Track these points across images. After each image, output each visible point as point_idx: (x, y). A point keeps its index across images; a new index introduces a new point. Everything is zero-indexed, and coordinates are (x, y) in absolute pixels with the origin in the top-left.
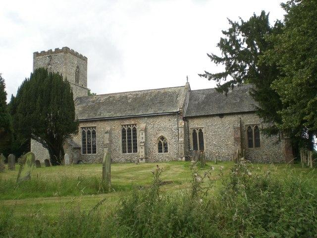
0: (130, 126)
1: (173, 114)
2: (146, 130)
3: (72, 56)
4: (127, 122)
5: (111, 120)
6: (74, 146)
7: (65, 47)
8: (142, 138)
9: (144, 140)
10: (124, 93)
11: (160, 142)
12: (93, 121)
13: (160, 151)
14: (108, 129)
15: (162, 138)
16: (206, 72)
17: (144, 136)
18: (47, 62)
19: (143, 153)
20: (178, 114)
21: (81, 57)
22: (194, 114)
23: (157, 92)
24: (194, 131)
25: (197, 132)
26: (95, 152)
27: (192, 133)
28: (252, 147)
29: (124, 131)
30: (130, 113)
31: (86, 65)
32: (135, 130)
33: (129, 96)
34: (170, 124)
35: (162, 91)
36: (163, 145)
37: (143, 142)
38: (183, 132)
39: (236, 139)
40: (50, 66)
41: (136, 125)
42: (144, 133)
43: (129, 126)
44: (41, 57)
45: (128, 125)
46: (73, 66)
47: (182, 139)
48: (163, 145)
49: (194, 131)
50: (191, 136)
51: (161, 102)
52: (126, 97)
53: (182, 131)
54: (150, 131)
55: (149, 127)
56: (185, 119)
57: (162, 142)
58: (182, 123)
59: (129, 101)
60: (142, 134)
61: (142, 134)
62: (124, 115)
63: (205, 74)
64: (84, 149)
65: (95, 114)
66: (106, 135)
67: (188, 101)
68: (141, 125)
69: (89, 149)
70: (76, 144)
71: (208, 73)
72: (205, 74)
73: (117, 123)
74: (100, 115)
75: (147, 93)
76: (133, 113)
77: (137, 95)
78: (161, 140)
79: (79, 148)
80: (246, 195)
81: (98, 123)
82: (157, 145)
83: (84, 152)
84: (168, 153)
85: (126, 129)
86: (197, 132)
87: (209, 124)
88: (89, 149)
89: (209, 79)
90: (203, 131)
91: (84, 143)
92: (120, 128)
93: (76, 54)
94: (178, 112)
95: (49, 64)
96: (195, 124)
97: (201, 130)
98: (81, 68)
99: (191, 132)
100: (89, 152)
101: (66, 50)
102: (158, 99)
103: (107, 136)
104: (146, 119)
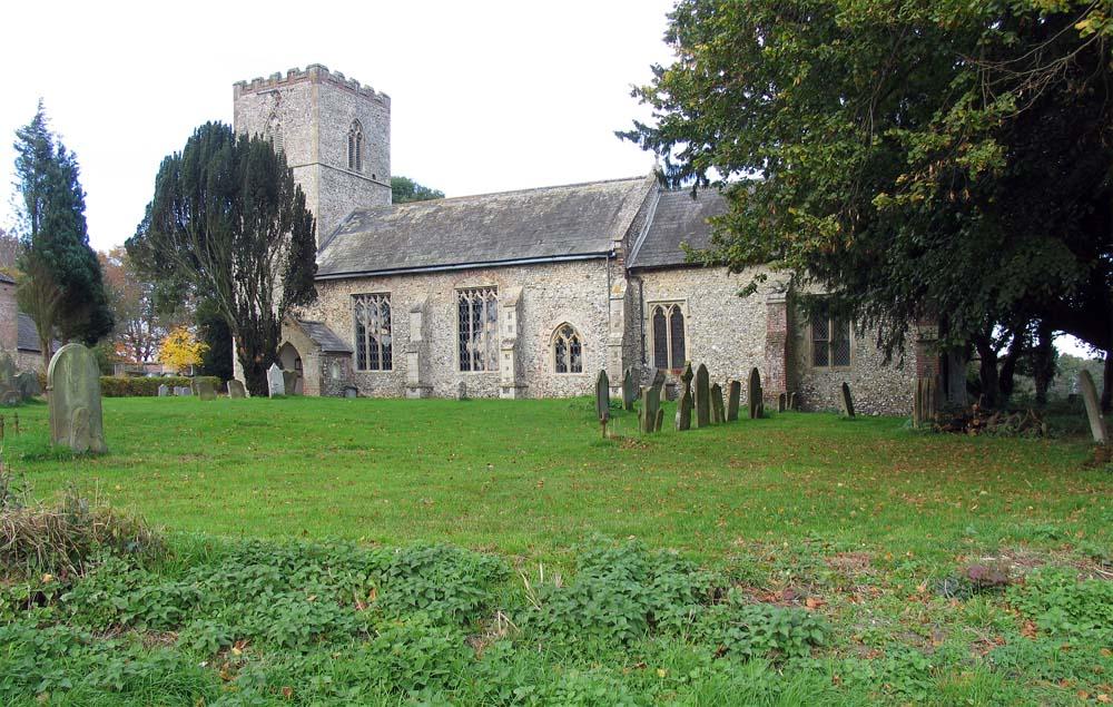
0: (467, 293)
1: (598, 259)
2: (520, 305)
3: (336, 93)
4: (471, 282)
5: (429, 273)
6: (330, 346)
7: (314, 66)
8: (510, 327)
9: (514, 335)
10: (479, 196)
11: (561, 340)
12: (383, 277)
13: (561, 368)
14: (421, 299)
15: (568, 330)
16: (636, 123)
17: (514, 321)
18: (268, 109)
19: (511, 373)
20: (612, 259)
21: (368, 94)
22: (657, 262)
23: (567, 192)
24: (659, 310)
25: (667, 313)
26: (388, 366)
27: (651, 318)
28: (826, 364)
29: (463, 306)
30: (478, 254)
31: (388, 118)
32: (477, 307)
33: (489, 207)
34: (591, 289)
35: (583, 192)
36: (471, 306)
37: (511, 341)
38: (622, 314)
39: (770, 338)
40: (276, 121)
41: (495, 289)
42: (514, 315)
43: (464, 294)
44: (252, 96)
45: (474, 291)
46: (340, 121)
47: (620, 335)
48: (471, 306)
49: (659, 310)
50: (649, 327)
51: (572, 225)
52: (481, 209)
53: (618, 308)
54: (532, 308)
55: (530, 297)
56: (633, 273)
57: (566, 340)
58: (621, 284)
59: (487, 221)
60: (510, 317)
61: (510, 317)
62: (463, 260)
63: (635, 129)
64: (362, 357)
65: (390, 257)
66: (414, 316)
67: (649, 220)
68: (511, 286)
69: (374, 357)
70: (338, 342)
71: (642, 128)
72: (635, 129)
73: (445, 282)
74: (402, 259)
75: (540, 198)
76: (494, 255)
77: (512, 202)
78: (564, 337)
79: (349, 354)
80: (829, 532)
81: (396, 281)
82: (552, 350)
83: (362, 366)
84: (582, 374)
85: (470, 300)
86: (667, 313)
87: (700, 292)
88: (374, 357)
89: (645, 148)
90: (684, 311)
91: (361, 339)
92: (454, 299)
93: (352, 87)
94: (610, 253)
95: (273, 116)
96: (660, 290)
97: (677, 309)
98: (370, 127)
99: (649, 312)
100: (375, 366)
101: (320, 74)
102: (566, 215)
103: (416, 319)
104: (523, 271)
